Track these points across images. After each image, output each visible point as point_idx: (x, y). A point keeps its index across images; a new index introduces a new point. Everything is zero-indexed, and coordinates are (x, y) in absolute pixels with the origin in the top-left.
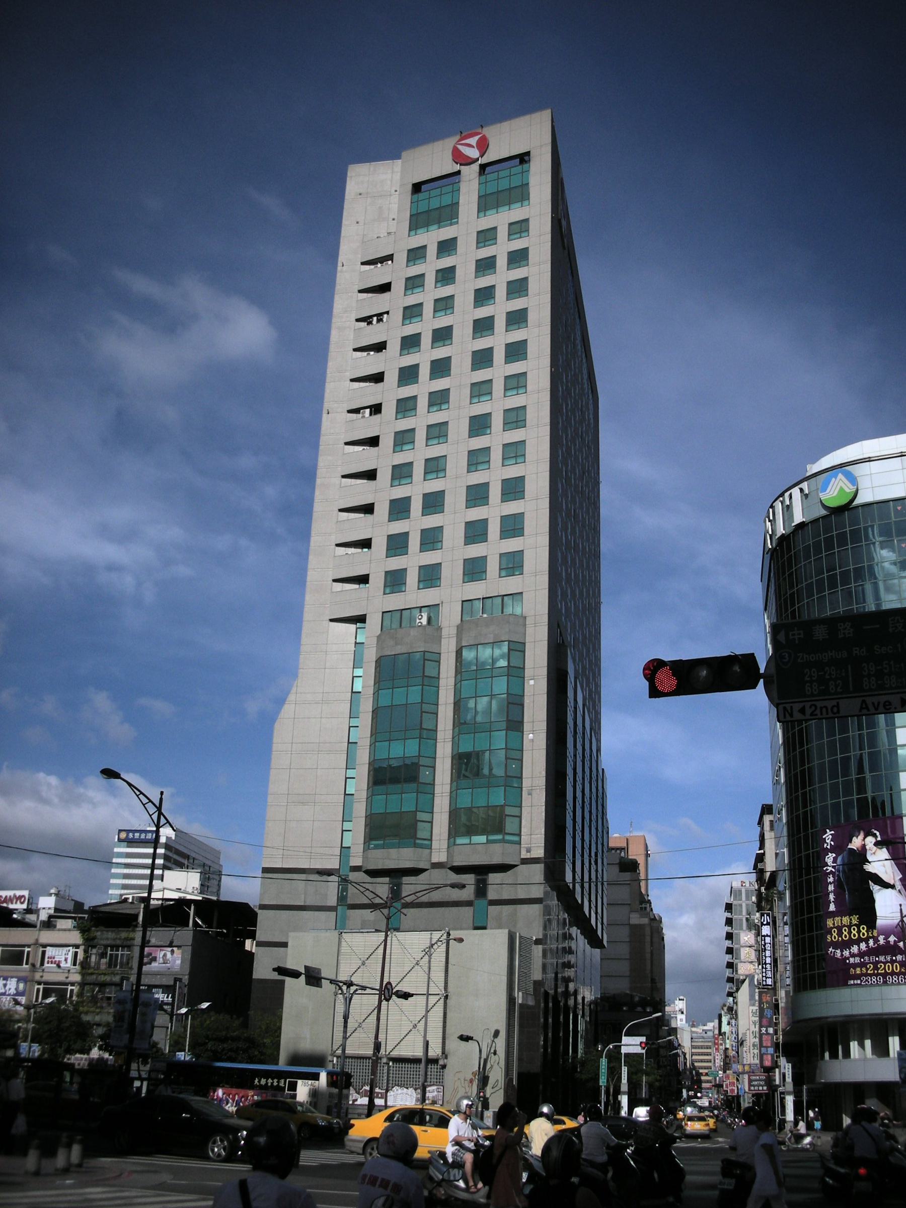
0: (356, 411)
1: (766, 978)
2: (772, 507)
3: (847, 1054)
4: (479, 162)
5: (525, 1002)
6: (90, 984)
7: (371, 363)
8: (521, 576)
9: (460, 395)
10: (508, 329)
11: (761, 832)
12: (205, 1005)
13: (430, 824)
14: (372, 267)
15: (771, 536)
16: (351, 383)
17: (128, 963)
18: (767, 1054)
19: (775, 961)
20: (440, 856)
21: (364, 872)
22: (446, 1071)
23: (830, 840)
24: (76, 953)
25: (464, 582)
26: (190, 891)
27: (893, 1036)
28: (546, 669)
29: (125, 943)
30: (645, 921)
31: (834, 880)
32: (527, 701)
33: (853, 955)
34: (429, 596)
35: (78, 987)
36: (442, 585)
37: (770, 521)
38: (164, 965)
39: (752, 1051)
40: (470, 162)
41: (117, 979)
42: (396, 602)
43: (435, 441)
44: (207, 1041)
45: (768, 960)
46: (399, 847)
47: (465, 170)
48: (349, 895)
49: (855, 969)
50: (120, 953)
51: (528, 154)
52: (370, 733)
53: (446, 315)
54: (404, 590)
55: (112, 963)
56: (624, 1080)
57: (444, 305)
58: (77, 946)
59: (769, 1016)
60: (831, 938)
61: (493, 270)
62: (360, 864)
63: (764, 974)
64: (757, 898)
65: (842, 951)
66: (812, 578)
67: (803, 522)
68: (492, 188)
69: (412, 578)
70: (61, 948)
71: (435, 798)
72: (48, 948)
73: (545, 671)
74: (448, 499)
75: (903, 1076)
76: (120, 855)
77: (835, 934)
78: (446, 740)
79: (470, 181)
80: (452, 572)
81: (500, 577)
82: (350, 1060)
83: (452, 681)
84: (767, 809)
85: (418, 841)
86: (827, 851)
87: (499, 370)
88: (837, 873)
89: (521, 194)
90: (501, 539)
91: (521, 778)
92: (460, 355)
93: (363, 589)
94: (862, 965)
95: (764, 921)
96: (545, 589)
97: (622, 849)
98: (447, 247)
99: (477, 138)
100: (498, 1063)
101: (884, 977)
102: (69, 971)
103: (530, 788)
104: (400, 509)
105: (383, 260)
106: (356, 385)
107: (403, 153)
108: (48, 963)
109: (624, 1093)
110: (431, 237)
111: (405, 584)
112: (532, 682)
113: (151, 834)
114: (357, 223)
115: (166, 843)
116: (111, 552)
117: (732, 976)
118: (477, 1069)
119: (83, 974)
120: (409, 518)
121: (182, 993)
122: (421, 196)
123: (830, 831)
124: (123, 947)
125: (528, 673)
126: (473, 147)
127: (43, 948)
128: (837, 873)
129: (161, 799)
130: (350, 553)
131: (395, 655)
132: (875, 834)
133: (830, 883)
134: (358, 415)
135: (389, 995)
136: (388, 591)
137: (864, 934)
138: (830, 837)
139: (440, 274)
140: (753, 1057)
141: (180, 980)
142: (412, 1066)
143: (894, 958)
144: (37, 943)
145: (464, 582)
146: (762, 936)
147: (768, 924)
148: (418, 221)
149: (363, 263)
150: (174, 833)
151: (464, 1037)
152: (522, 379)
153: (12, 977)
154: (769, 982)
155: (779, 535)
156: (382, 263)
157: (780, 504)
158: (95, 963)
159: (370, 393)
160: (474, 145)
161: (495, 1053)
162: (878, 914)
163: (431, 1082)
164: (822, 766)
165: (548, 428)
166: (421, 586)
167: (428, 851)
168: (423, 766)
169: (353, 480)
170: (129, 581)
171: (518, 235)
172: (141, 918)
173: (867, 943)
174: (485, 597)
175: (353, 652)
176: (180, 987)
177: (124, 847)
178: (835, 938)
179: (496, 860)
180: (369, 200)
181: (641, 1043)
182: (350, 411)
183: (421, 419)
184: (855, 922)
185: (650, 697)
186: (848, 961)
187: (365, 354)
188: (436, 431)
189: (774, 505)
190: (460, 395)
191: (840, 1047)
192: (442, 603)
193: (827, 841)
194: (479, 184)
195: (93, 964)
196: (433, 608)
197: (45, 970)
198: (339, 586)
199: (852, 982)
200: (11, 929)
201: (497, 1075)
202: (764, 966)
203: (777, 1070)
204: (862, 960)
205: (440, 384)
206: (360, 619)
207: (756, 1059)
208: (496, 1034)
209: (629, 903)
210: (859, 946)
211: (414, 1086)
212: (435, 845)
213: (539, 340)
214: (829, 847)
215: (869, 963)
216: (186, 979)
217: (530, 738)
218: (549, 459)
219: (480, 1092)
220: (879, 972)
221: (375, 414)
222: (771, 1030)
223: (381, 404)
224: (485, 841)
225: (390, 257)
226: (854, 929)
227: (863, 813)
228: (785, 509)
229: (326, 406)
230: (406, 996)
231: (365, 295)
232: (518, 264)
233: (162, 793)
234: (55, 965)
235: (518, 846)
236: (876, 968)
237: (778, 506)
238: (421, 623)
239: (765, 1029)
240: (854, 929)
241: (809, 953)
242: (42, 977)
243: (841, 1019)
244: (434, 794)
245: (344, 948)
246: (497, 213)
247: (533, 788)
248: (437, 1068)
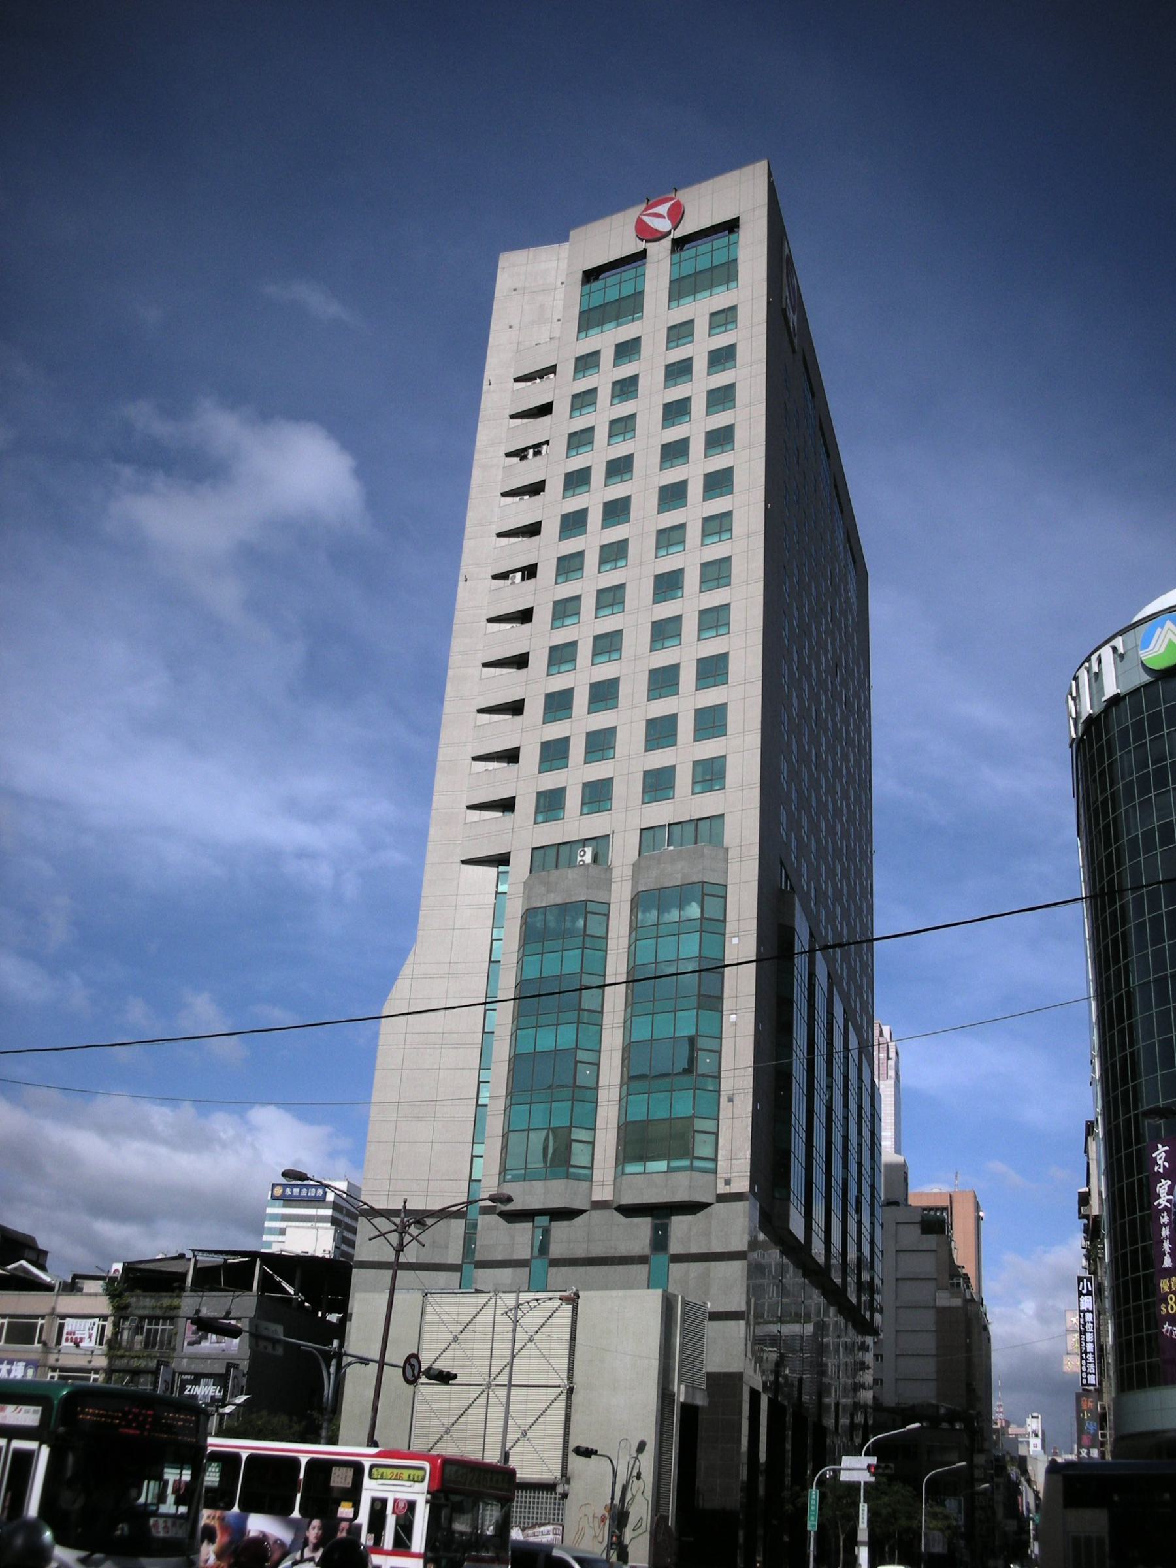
0: (504, 576)
2: (1076, 678)
4: (672, 236)
5: (690, 1401)
6: (119, 1371)
9: (642, 545)
10: (709, 454)
14: (529, 384)
15: (1076, 721)
16: (499, 539)
17: (170, 1342)
20: (603, 1191)
21: (498, 1214)
22: (568, 1502)
23: (1163, 1160)
24: (103, 1327)
25: (643, 803)
28: (755, 922)
29: (167, 1314)
31: (1170, 1220)
34: (595, 825)
35: (103, 1375)
36: (613, 808)
37: (1074, 699)
38: (217, 1345)
40: (659, 237)
41: (153, 1364)
42: (550, 833)
43: (608, 611)
47: (652, 248)
48: (477, 1248)
50: (160, 1327)
53: (624, 440)
55: (149, 1343)
56: (863, 1525)
57: (623, 427)
58: (105, 1318)
59: (1092, 1432)
60: (1167, 1308)
61: (689, 376)
63: (1084, 1369)
66: (1131, 774)
69: (573, 800)
70: (84, 1321)
71: (599, 1108)
72: (68, 1319)
73: (753, 925)
74: (624, 690)
76: (275, 1217)
78: (615, 1026)
79: (658, 261)
80: (628, 789)
81: (693, 794)
83: (624, 942)
85: (572, 1170)
86: (1159, 1177)
89: (727, 273)
90: (695, 741)
95: (1083, 1289)
97: (944, 1209)
98: (627, 350)
99: (668, 205)
100: (643, 1492)
102: (93, 1352)
103: (731, 1092)
104: (558, 705)
105: (542, 374)
106: (505, 541)
107: (571, 233)
108: (67, 1340)
109: (863, 1544)
110: (605, 340)
112: (735, 941)
113: (314, 1190)
114: (511, 327)
115: (334, 1202)
116: (303, 834)
118: (610, 1501)
119: (111, 1357)
121: (238, 1385)
122: (596, 285)
123: (1163, 1146)
124: (165, 1319)
125: (730, 927)
126: (664, 217)
127: (61, 1319)
131: (546, 907)
133: (1165, 1225)
134: (506, 581)
135: (413, 1375)
136: (540, 818)
138: (1164, 1155)
139: (618, 388)
141: (236, 1366)
142: (545, 1495)
144: (53, 1313)
145: (643, 803)
147: (1089, 1293)
148: (590, 319)
149: (517, 380)
151: (582, 1450)
152: (725, 521)
153: (19, 1360)
154: (1092, 1379)
155: (1084, 716)
156: (541, 377)
157: (1086, 672)
158: (128, 1342)
160: (665, 214)
161: (638, 1477)
163: (545, 1519)
164: (1150, 1049)
166: (585, 811)
167: (586, 1184)
169: (497, 669)
170: (323, 873)
171: (723, 329)
172: (189, 1279)
173: (936, 1212)
174: (671, 822)
175: (493, 906)
176: (235, 1377)
177: (279, 1207)
179: (680, 1196)
181: (869, 1467)
182: (495, 577)
187: (517, 499)
188: (609, 598)
193: (1159, 1162)
194: (671, 265)
195: (124, 1343)
196: (600, 843)
197: (62, 1351)
198: (476, 815)
200: (21, 1292)
201: (640, 1510)
202: (1084, 1355)
205: (616, 534)
206: (502, 860)
209: (934, 1277)
211: (522, 1525)
212: (597, 1175)
214: (1161, 1170)
216: (244, 1365)
217: (731, 1020)
219: (612, 1536)
223: (536, 565)
224: (665, 1169)
225: (552, 369)
229: (463, 571)
230: (445, 1378)
231: (518, 422)
232: (721, 367)
234: (72, 1344)
235: (712, 1176)
237: (1084, 676)
239: (1085, 1451)
241: (1135, 1333)
242: (57, 1360)
244: (597, 1103)
245: (430, 1317)
247: (735, 1092)
248: (555, 1499)
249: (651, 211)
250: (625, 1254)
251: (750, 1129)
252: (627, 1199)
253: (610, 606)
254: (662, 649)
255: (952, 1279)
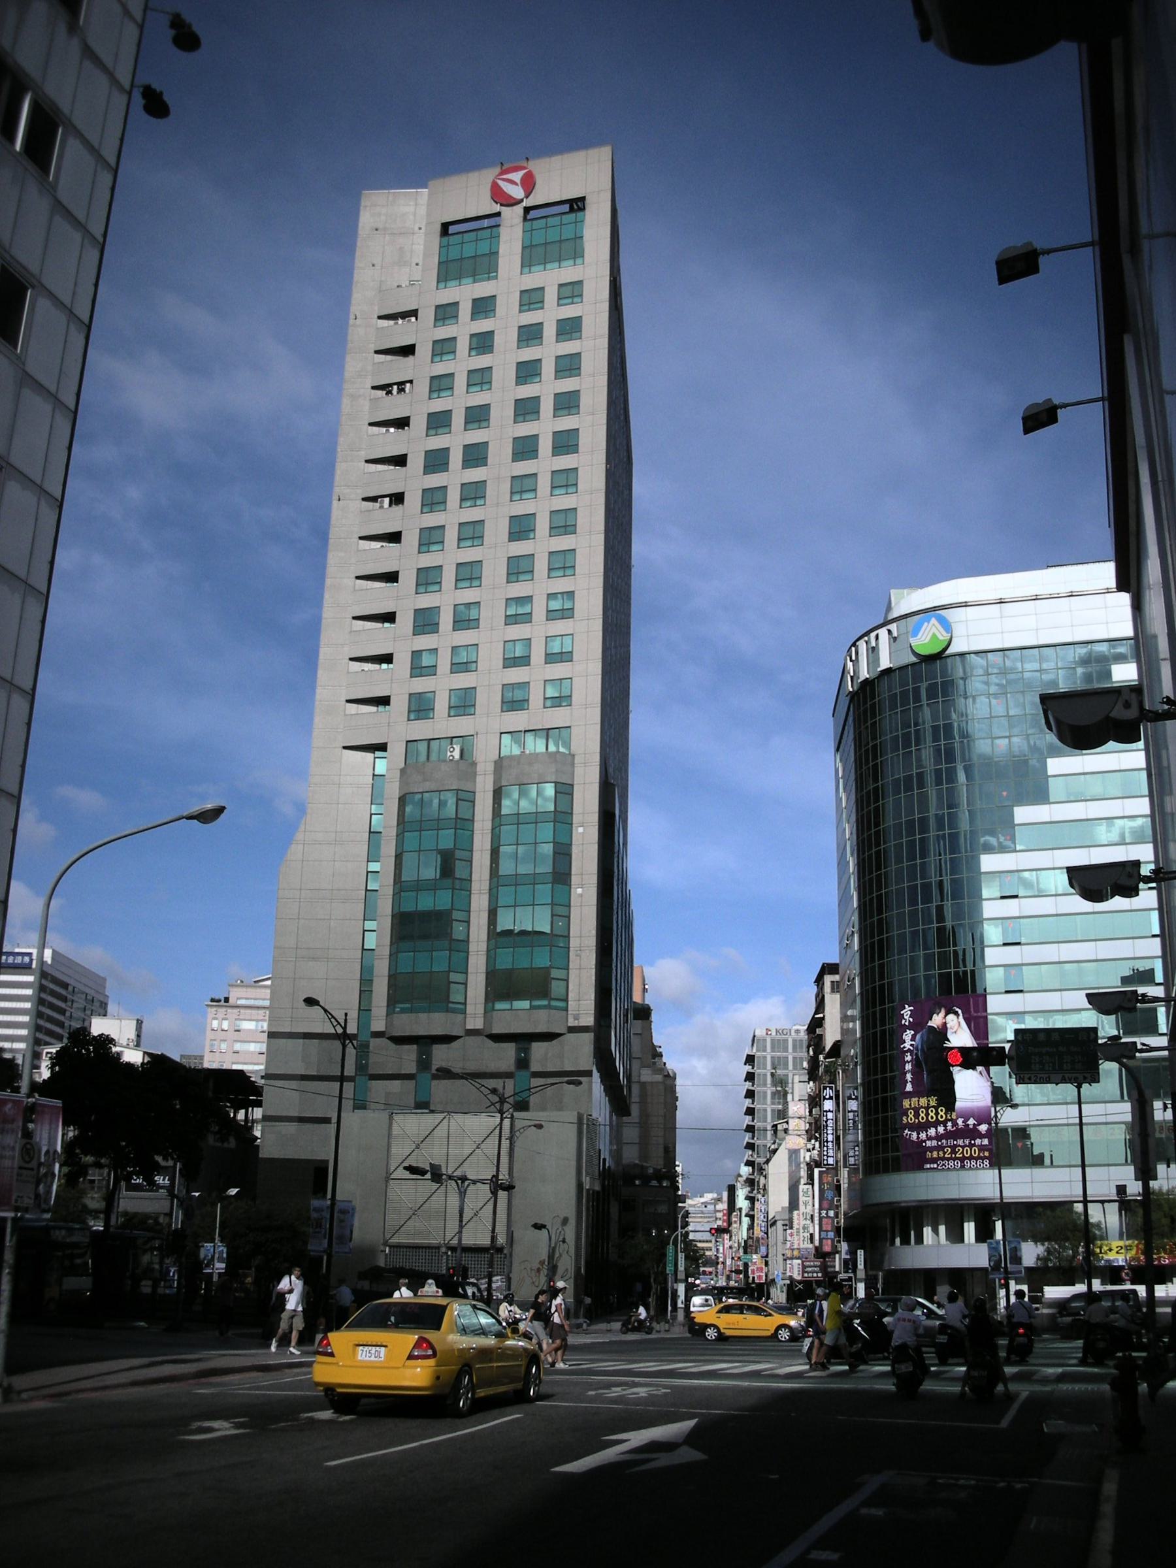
0: (374, 499)
1: (828, 1157)
3: (920, 1239)
4: (524, 204)
7: (391, 442)
8: (568, 707)
9: (499, 490)
11: (817, 996)
12: (233, 1192)
13: (463, 986)
16: (367, 464)
18: (828, 1239)
19: (838, 1138)
20: (475, 1021)
21: (388, 1038)
26: (125, 1044)
27: (969, 1221)
30: (659, 1078)
32: (575, 851)
33: (930, 1138)
34: (461, 726)
36: (477, 713)
37: (851, 660)
39: (802, 1235)
40: (512, 202)
42: (421, 729)
44: (248, 1232)
45: (830, 1138)
46: (429, 1012)
47: (506, 211)
49: (931, 1152)
51: (583, 199)
52: (392, 881)
54: (431, 716)
62: (383, 1029)
64: (808, 1063)
65: (918, 1134)
67: (891, 668)
68: (538, 238)
75: (992, 1264)
77: (911, 1116)
80: (488, 699)
82: (405, 1250)
83: (489, 825)
84: (829, 969)
85: (451, 1005)
86: (904, 1028)
87: (545, 463)
88: (915, 1052)
89: (572, 249)
91: (568, 937)
92: (498, 441)
93: (383, 714)
94: (940, 1148)
96: (596, 724)
99: (521, 173)
101: (962, 1162)
105: (405, 315)
110: (464, 293)
111: (433, 709)
112: (581, 830)
114: (373, 265)
117: (753, 1141)
120: (438, 632)
128: (915, 1052)
129: (346, 1020)
130: (366, 669)
132: (957, 1012)
133: (908, 1062)
134: (375, 504)
137: (942, 1117)
138: (909, 1013)
140: (803, 1240)
143: (973, 1142)
146: (824, 1111)
147: (831, 1098)
150: (355, 1051)
152: (572, 475)
155: (862, 678)
157: (865, 644)
159: (389, 479)
160: (518, 181)
161: (564, 1241)
162: (958, 1095)
165: (602, 536)
167: (461, 1016)
168: (457, 920)
169: (369, 582)
171: (570, 300)
173: (945, 1126)
178: (911, 1119)
179: (541, 1028)
180: (387, 237)
183: (452, 516)
184: (933, 1103)
185: (1117, 1186)
186: (924, 1144)
189: (857, 644)
190: (499, 490)
191: (912, 1233)
192: (477, 734)
193: (905, 1017)
196: (465, 741)
198: (353, 708)
199: (928, 1166)
201: (567, 1262)
203: (837, 1256)
204: (940, 1143)
207: (806, 1243)
208: (565, 1221)
210: (936, 1129)
212: (470, 1009)
213: (593, 431)
214: (907, 1024)
215: (946, 1147)
218: (602, 574)
220: (957, 1156)
221: (396, 504)
222: (831, 1213)
224: (528, 1007)
225: (414, 313)
226: (932, 1111)
227: (945, 989)
228: (870, 651)
233: (346, 1014)
236: (954, 1152)
237: (862, 645)
238: (453, 757)
239: (825, 1212)
240: (932, 1111)
243: (914, 1204)
246: (545, 270)
249: (504, 177)
250: (495, 1071)
251: (594, 978)
252: (496, 1030)
253: (470, 538)
254: (517, 582)
255: (654, 1059)
